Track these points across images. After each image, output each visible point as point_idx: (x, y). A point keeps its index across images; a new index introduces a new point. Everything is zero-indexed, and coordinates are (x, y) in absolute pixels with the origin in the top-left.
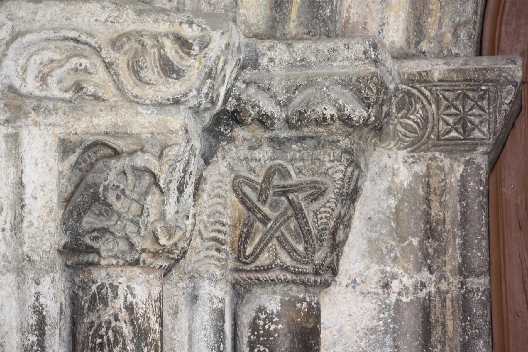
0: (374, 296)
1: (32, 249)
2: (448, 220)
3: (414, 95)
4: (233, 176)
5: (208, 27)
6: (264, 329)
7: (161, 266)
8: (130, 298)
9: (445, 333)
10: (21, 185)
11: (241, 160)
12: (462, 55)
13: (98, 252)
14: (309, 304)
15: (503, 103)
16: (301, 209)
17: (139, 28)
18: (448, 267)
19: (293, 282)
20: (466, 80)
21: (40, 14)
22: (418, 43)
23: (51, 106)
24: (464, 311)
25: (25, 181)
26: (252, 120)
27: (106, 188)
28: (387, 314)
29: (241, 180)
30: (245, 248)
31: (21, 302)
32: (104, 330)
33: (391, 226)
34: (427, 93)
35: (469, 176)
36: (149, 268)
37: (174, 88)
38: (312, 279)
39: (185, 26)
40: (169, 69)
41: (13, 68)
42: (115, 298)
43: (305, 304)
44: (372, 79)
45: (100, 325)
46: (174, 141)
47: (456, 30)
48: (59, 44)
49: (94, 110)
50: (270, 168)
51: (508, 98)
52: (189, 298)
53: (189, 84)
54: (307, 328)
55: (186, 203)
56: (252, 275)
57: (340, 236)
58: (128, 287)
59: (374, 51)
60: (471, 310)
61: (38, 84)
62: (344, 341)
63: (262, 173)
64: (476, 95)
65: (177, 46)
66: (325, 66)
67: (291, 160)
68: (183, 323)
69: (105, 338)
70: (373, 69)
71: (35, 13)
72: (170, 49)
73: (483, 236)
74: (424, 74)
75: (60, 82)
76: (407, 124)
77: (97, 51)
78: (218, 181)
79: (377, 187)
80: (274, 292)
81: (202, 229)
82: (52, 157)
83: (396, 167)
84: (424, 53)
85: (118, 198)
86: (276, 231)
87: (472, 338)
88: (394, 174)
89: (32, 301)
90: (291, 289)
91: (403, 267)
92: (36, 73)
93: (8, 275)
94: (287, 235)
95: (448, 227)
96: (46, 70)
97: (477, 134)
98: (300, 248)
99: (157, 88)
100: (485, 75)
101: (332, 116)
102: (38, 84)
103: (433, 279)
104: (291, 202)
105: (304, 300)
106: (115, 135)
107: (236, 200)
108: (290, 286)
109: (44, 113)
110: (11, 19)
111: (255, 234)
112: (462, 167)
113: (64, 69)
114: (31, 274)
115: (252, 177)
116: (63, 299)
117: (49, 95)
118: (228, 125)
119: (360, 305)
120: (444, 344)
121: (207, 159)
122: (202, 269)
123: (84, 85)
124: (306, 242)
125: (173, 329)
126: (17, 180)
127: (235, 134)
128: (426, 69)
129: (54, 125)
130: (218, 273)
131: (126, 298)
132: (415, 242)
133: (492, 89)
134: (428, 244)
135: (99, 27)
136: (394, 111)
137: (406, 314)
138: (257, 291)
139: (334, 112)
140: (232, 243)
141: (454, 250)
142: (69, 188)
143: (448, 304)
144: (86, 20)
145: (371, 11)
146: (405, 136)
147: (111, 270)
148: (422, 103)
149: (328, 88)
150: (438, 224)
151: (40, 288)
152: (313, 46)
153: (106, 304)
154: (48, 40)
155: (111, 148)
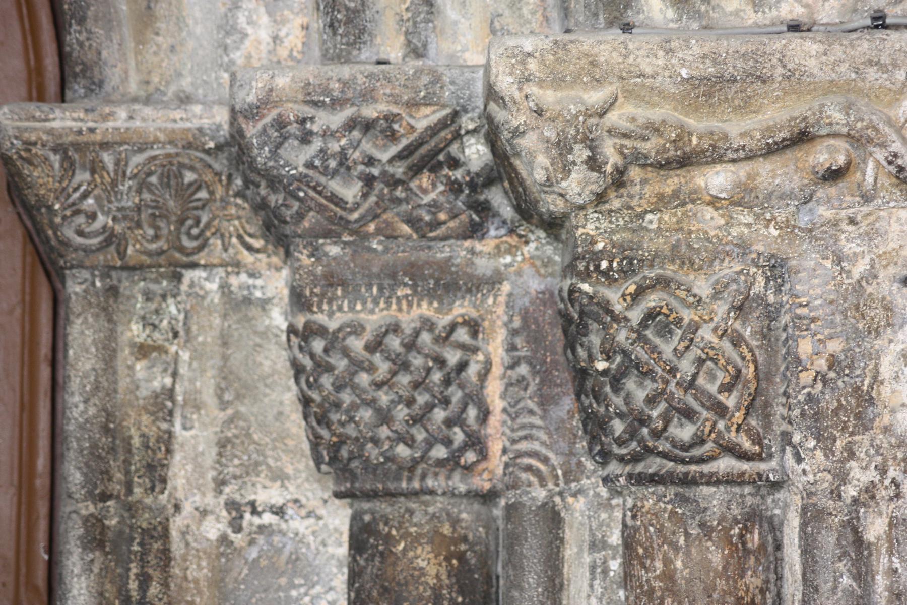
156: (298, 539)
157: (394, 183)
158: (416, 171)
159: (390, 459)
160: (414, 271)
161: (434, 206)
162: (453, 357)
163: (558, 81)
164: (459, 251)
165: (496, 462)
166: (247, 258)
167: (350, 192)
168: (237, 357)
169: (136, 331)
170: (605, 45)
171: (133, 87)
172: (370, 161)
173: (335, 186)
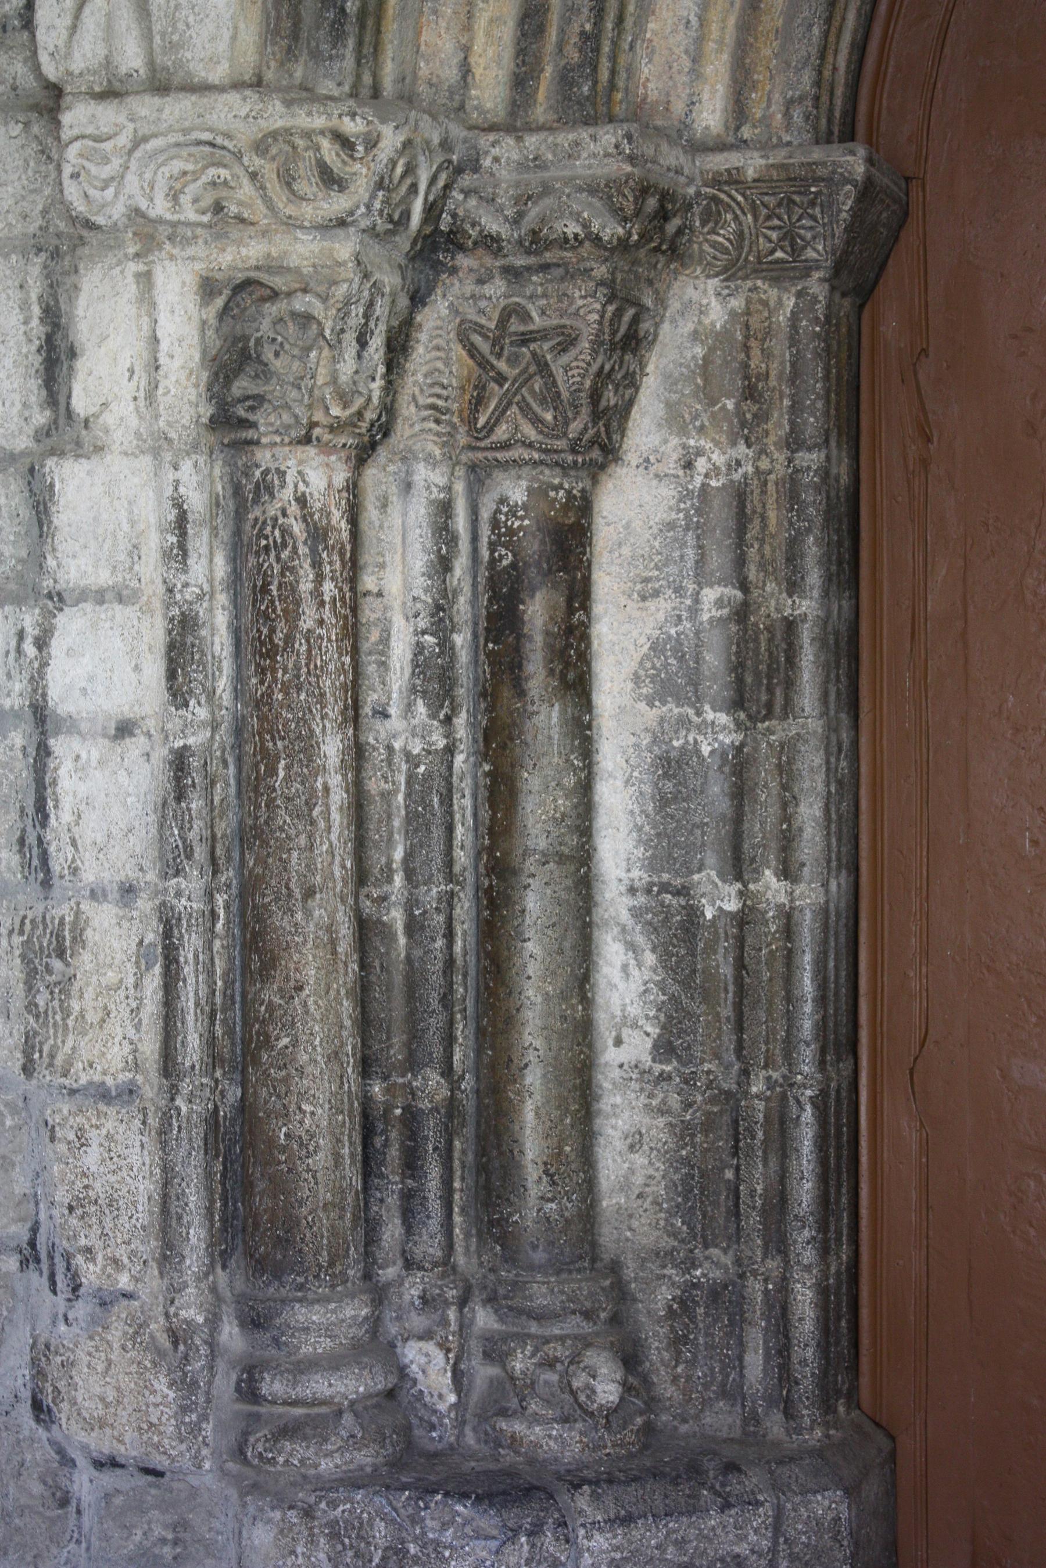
0: (673, 479)
1: (169, 424)
2: (773, 374)
3: (722, 201)
4: (458, 320)
5: (376, 121)
6: (506, 526)
7: (344, 445)
8: (302, 487)
9: (764, 526)
10: (155, 340)
11: (468, 299)
12: (795, 143)
13: (253, 425)
14: (569, 492)
15: (840, 211)
16: (546, 364)
17: (289, 124)
18: (772, 438)
19: (542, 462)
20: (790, 179)
21: (167, 111)
22: (738, 128)
23: (189, 234)
24: (791, 498)
25: (159, 334)
26: (475, 243)
27: (258, 341)
28: (689, 503)
29: (467, 325)
30: (476, 419)
31: (159, 491)
32: (269, 528)
33: (696, 384)
34: (740, 198)
35: (802, 312)
36: (327, 449)
37: (338, 204)
38: (570, 458)
39: (346, 119)
40: (330, 179)
41: (136, 184)
42: (283, 487)
43: (561, 493)
44: (626, 182)
45: (264, 522)
46: (343, 276)
47: (788, 109)
48: (193, 149)
49: (242, 238)
50: (504, 309)
51: (846, 201)
52: (402, 486)
53: (356, 198)
54: (564, 525)
55: (371, 359)
56: (490, 455)
57: (610, 397)
58: (299, 472)
59: (629, 143)
60: (799, 496)
61: (170, 205)
62: (632, 540)
63: (496, 316)
64: (805, 200)
65: (337, 147)
66: (565, 167)
67: (531, 297)
68: (395, 517)
69: (271, 539)
70: (629, 169)
71: (160, 110)
72: (329, 150)
73: (818, 394)
74: (734, 172)
75: (195, 201)
76: (716, 242)
77: (238, 156)
78: (437, 328)
79: (680, 331)
80: (519, 477)
81: (417, 393)
82: (191, 302)
83: (705, 302)
84: (745, 142)
85: (277, 354)
86: (515, 394)
87: (798, 531)
88: (701, 312)
89: (169, 491)
90: (542, 472)
91: (713, 440)
92: (166, 189)
93: (141, 457)
94: (530, 400)
95: (773, 382)
96: (178, 186)
97: (810, 254)
98: (549, 417)
99: (316, 204)
100: (814, 171)
101: (576, 235)
102: (170, 205)
103: (751, 454)
104: (534, 354)
105: (561, 486)
106: (269, 269)
107: (464, 353)
108: (541, 468)
109: (181, 242)
110: (132, 120)
111: (489, 398)
112: (793, 300)
113: (199, 183)
114: (168, 457)
115: (483, 321)
116: (219, 488)
117: (183, 219)
118: (448, 250)
119: (654, 492)
120: (762, 542)
121: (418, 299)
122: (418, 447)
123: (224, 204)
124: (555, 409)
125: (381, 527)
126: (150, 333)
127: (458, 263)
128: (737, 165)
129: (192, 259)
130: (437, 452)
131: (296, 486)
132: (730, 405)
133: (825, 191)
134: (745, 408)
135: (239, 125)
136: (697, 224)
137: (716, 503)
138: (499, 475)
139: (578, 230)
140: (461, 412)
141: (781, 415)
142: (217, 342)
143: (771, 487)
144: (222, 116)
145: (675, 86)
146: (714, 258)
147: (277, 450)
148: (734, 212)
149: (568, 196)
150: (758, 380)
151: (178, 475)
152: (550, 139)
153: (272, 495)
154: (178, 145)
155: (271, 288)
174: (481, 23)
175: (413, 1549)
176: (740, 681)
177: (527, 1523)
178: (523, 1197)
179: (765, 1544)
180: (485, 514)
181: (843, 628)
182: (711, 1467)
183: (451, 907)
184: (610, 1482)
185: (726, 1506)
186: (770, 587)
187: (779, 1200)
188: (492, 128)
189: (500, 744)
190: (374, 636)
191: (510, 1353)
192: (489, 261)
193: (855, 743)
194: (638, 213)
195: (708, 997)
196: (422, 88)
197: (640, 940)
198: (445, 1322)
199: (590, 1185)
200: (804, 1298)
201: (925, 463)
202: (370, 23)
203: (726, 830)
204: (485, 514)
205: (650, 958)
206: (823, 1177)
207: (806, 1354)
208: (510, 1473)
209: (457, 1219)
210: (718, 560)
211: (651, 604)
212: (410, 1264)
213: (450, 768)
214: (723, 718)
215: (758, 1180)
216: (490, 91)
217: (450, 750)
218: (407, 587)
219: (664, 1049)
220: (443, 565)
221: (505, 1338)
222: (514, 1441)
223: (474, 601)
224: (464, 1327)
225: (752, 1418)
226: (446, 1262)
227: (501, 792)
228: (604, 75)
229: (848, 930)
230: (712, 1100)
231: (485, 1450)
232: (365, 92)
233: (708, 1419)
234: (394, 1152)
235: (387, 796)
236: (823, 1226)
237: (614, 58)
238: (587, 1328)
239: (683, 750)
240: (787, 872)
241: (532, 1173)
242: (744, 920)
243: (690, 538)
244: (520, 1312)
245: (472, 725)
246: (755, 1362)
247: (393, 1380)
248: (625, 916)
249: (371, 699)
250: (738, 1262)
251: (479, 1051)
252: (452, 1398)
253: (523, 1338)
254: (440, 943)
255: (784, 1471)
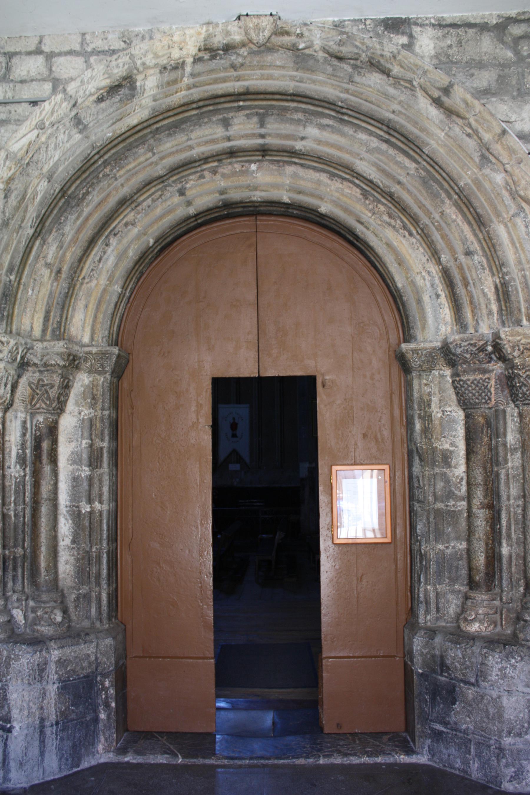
51: (114, 359)
57: (62, 398)
97: (106, 369)
98: (48, 403)
121: (19, 376)
132: (89, 401)
138: (37, 415)
156: (454, 417)
157: (476, 354)
158: (479, 352)
159: (475, 402)
160: (479, 369)
161: (483, 358)
162: (486, 384)
163: (512, 336)
164: (486, 366)
165: (493, 402)
166: (443, 368)
167: (468, 356)
168: (442, 385)
169: (424, 381)
170: (519, 329)
171: (422, 340)
172: (472, 351)
173: (465, 355)
174: (36, 318)
175: (12, 656)
176: (90, 460)
177: (39, 649)
178: (41, 576)
179: (94, 651)
180: (34, 424)
181: (114, 449)
182: (82, 634)
183: (24, 511)
184: (59, 639)
185: (86, 643)
186: (97, 440)
187: (98, 575)
188: (37, 340)
189: (36, 474)
190: (8, 450)
191: (37, 611)
192: (35, 369)
193: (117, 474)
194: (68, 359)
195: (83, 530)
196: (22, 331)
197: (68, 517)
198: (22, 605)
199: (56, 572)
200: (104, 596)
201: (132, 414)
202: (10, 317)
203: (87, 493)
204: (34, 424)
205: (70, 522)
206: (109, 569)
207: (105, 608)
208: (36, 638)
209: (26, 581)
210: (86, 434)
211: (71, 444)
212: (14, 592)
213: (25, 480)
214: (87, 469)
215: (94, 570)
216: (37, 332)
217: (25, 476)
218: (16, 440)
219: (73, 542)
220: (24, 435)
221: (36, 607)
222: (38, 631)
223: (31, 443)
224: (27, 606)
225: (93, 623)
226: (23, 591)
227: (36, 485)
228: (62, 330)
229: (115, 515)
230: (84, 553)
231: (31, 633)
232: (8, 332)
233: (83, 624)
234: (11, 566)
235: (10, 486)
236: (109, 580)
237: (65, 326)
238: (55, 604)
239: (78, 476)
240: (101, 502)
241: (43, 570)
242: (91, 513)
243: (80, 429)
244: (40, 602)
245: (30, 470)
246: (93, 610)
247: (9, 618)
248: (65, 512)
249: (7, 464)
250: (90, 588)
251: (31, 543)
252: (24, 622)
253: (40, 607)
254: (22, 519)
255: (99, 634)
